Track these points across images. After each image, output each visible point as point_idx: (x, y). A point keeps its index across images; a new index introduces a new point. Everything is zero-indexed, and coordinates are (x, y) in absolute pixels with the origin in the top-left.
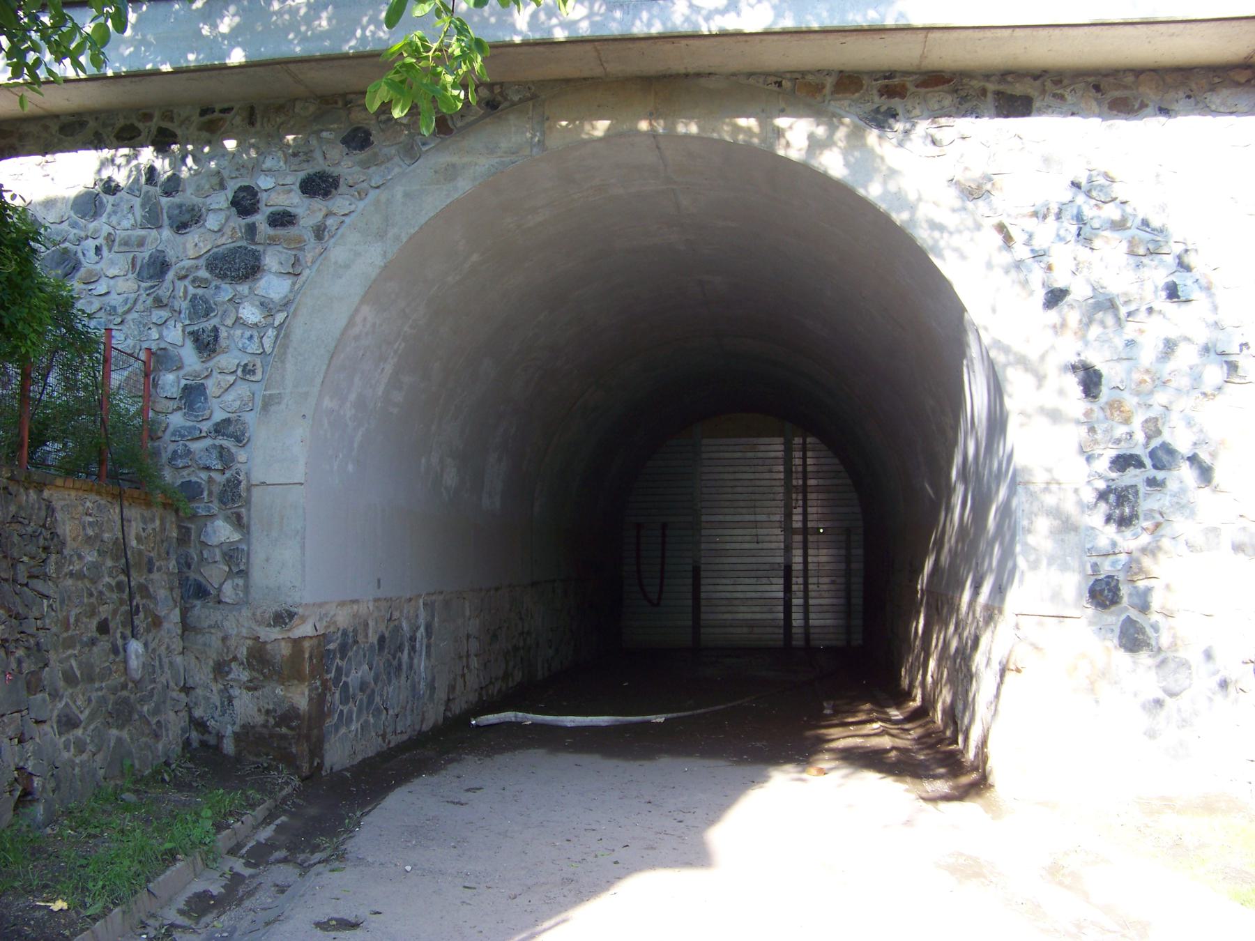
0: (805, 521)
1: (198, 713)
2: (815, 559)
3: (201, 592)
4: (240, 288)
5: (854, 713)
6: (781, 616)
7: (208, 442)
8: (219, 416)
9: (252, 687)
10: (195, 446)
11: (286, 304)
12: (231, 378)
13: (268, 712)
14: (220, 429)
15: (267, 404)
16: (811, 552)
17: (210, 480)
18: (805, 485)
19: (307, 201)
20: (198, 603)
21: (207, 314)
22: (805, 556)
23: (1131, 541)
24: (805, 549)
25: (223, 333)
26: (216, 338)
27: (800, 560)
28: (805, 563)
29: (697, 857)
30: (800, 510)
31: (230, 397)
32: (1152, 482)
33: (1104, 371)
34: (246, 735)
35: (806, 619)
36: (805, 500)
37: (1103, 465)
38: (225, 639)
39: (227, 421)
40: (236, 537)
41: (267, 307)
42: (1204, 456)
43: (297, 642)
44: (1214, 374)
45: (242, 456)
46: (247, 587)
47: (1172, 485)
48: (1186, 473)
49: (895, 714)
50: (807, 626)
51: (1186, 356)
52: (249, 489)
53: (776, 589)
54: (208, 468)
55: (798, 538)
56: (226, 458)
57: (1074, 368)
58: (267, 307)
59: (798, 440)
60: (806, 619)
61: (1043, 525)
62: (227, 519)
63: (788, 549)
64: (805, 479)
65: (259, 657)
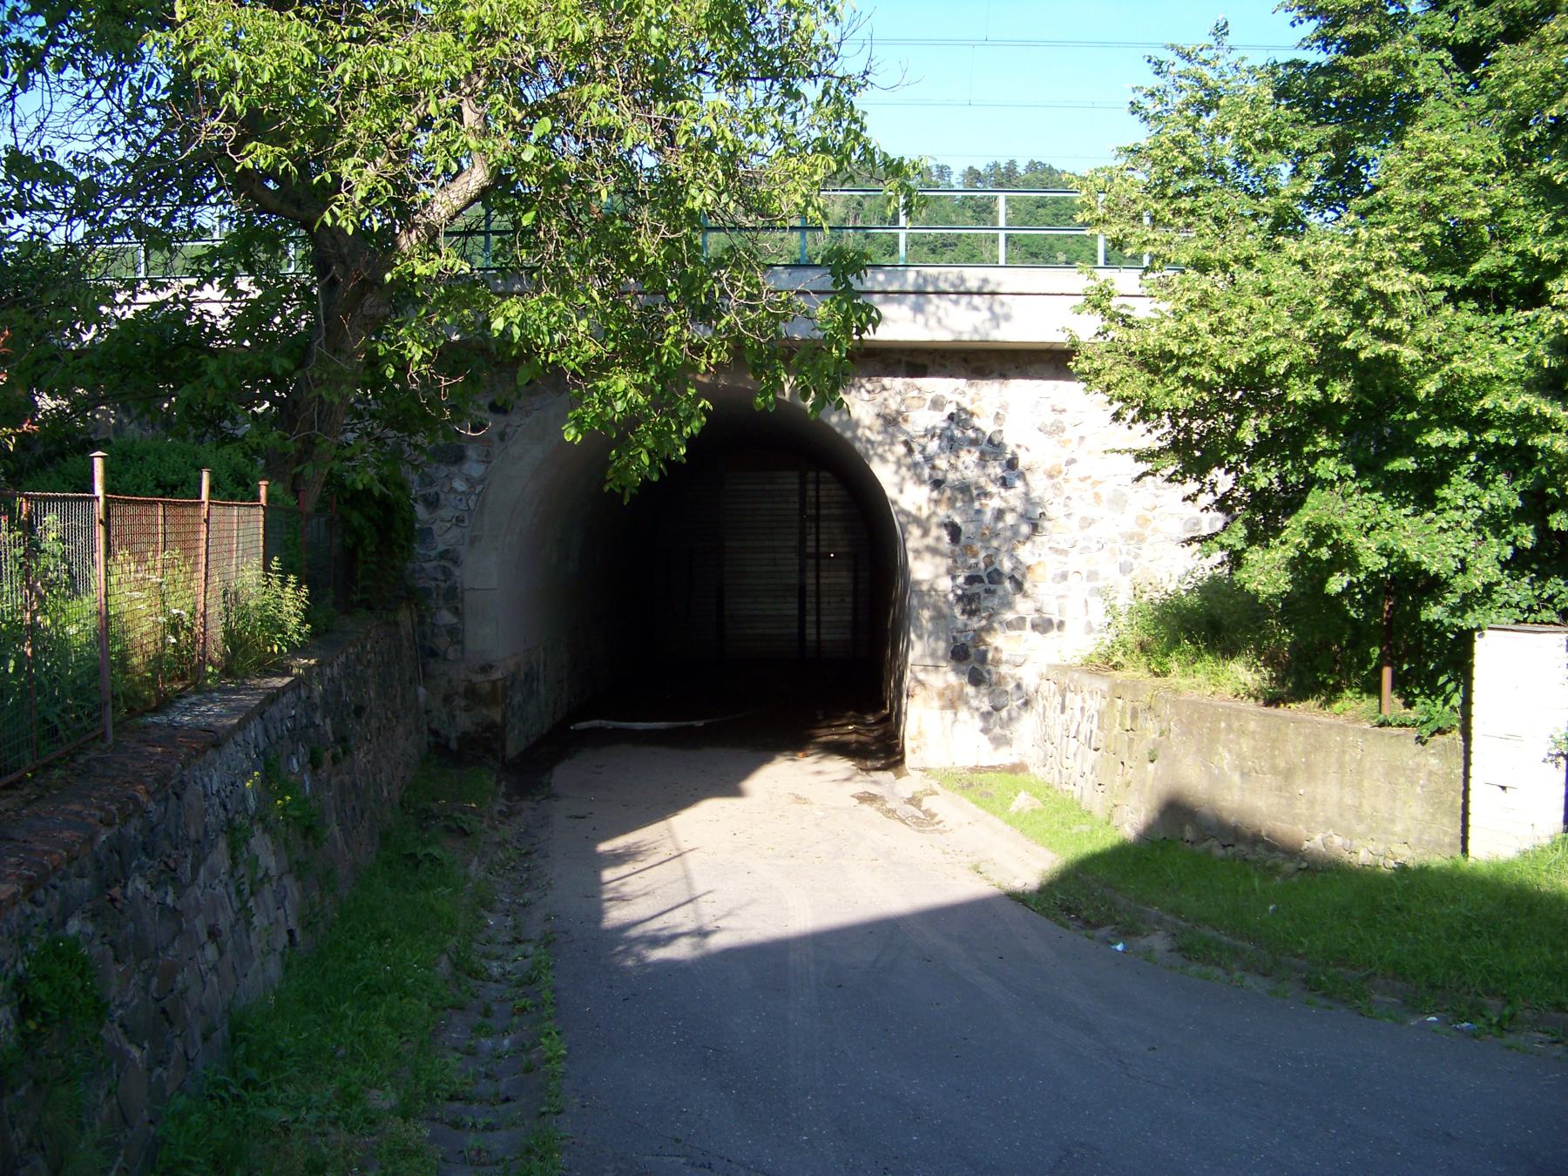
0: (817, 546)
1: (434, 725)
2: (826, 581)
3: (433, 653)
4: (452, 469)
5: (839, 718)
6: (796, 631)
7: (435, 563)
8: (441, 548)
9: (467, 710)
10: (427, 565)
11: (482, 480)
12: (449, 525)
13: (478, 724)
14: (443, 555)
15: (473, 541)
16: (822, 574)
17: (438, 586)
18: (818, 515)
19: (493, 416)
20: (432, 661)
21: (431, 483)
22: (818, 577)
23: (976, 623)
24: (818, 571)
25: (442, 497)
26: (438, 499)
27: (813, 581)
28: (818, 584)
29: (737, 793)
30: (813, 537)
31: (448, 536)
32: (988, 591)
33: (963, 528)
34: (464, 738)
35: (818, 634)
36: (817, 527)
37: (961, 580)
38: (450, 681)
39: (447, 551)
40: (455, 620)
41: (469, 480)
42: (1018, 576)
43: (494, 683)
44: (1025, 529)
45: (457, 572)
46: (463, 651)
47: (1001, 593)
48: (1008, 585)
49: (870, 719)
50: (818, 641)
51: (1010, 519)
52: (462, 592)
53: (791, 607)
54: (436, 579)
55: (812, 562)
56: (447, 573)
57: (946, 526)
58: (469, 480)
59: (812, 475)
60: (818, 634)
61: (926, 614)
62: (449, 609)
63: (802, 571)
64: (818, 509)
65: (472, 692)
